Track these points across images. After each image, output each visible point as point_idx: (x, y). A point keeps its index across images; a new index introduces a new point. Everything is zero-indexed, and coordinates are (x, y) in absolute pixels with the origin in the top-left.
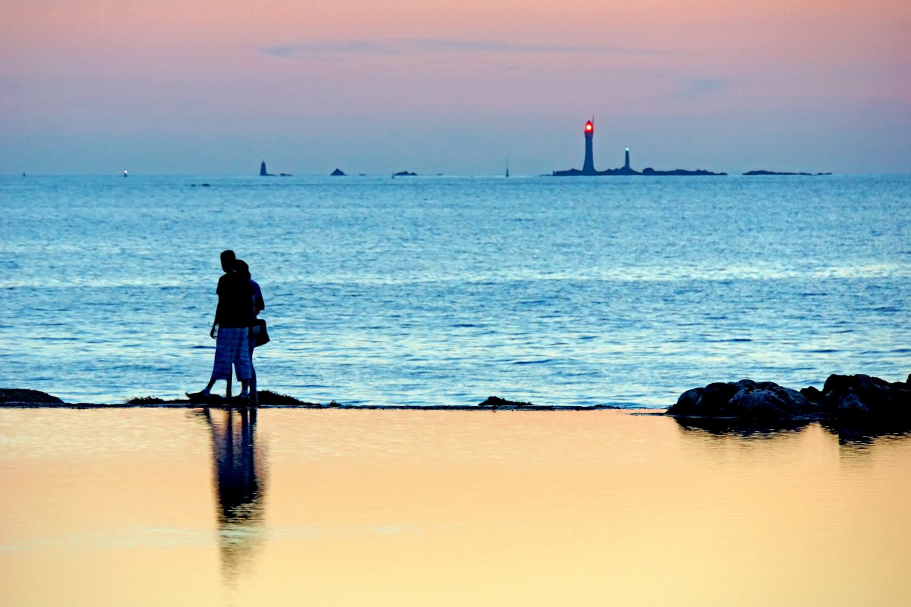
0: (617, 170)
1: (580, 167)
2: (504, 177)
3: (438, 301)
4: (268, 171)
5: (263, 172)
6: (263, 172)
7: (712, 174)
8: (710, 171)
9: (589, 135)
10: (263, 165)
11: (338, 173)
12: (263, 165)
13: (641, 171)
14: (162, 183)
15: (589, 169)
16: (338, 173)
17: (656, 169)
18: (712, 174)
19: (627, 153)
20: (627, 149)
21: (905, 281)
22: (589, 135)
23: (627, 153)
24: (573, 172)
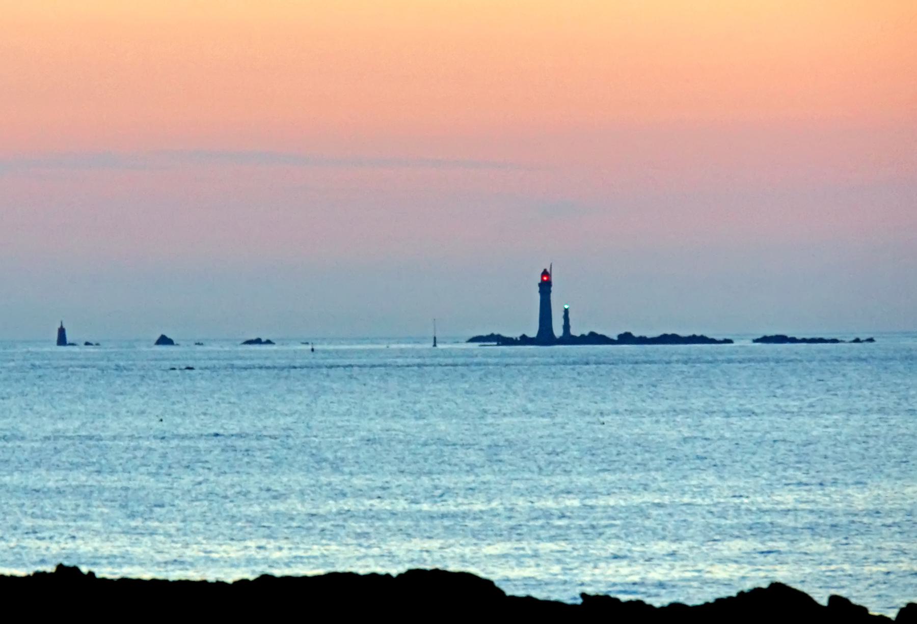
0: (583, 336)
1: (533, 333)
2: (430, 345)
3: (546, 500)
4: (69, 338)
5: (62, 340)
6: (62, 340)
7: (793, 340)
8: (710, 336)
9: (545, 287)
10: (62, 332)
11: (164, 340)
12: (62, 332)
13: (615, 337)
14: (260, 355)
15: (545, 337)
16: (164, 340)
17: (636, 334)
18: (793, 340)
19: (566, 311)
20: (566, 307)
21: (363, 526)
22: (545, 287)
23: (566, 311)
24: (525, 340)
